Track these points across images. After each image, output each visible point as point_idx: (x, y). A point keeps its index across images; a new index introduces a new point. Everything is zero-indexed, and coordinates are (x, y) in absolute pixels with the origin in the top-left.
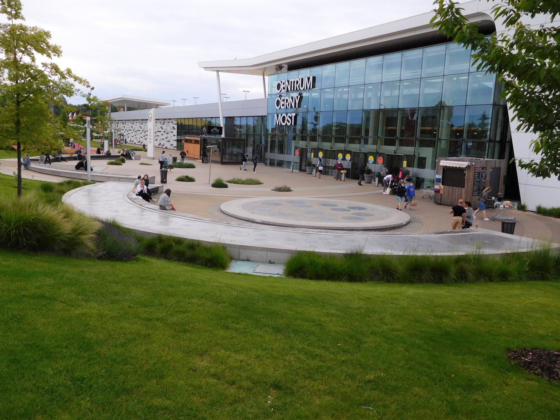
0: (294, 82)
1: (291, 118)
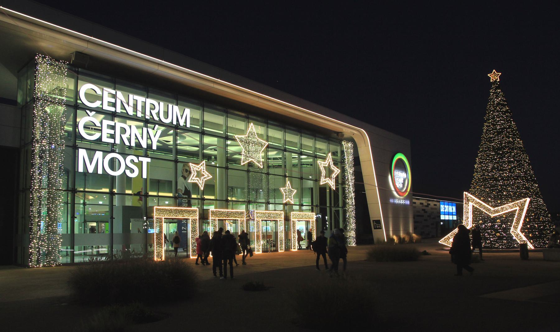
1: (140, 165)
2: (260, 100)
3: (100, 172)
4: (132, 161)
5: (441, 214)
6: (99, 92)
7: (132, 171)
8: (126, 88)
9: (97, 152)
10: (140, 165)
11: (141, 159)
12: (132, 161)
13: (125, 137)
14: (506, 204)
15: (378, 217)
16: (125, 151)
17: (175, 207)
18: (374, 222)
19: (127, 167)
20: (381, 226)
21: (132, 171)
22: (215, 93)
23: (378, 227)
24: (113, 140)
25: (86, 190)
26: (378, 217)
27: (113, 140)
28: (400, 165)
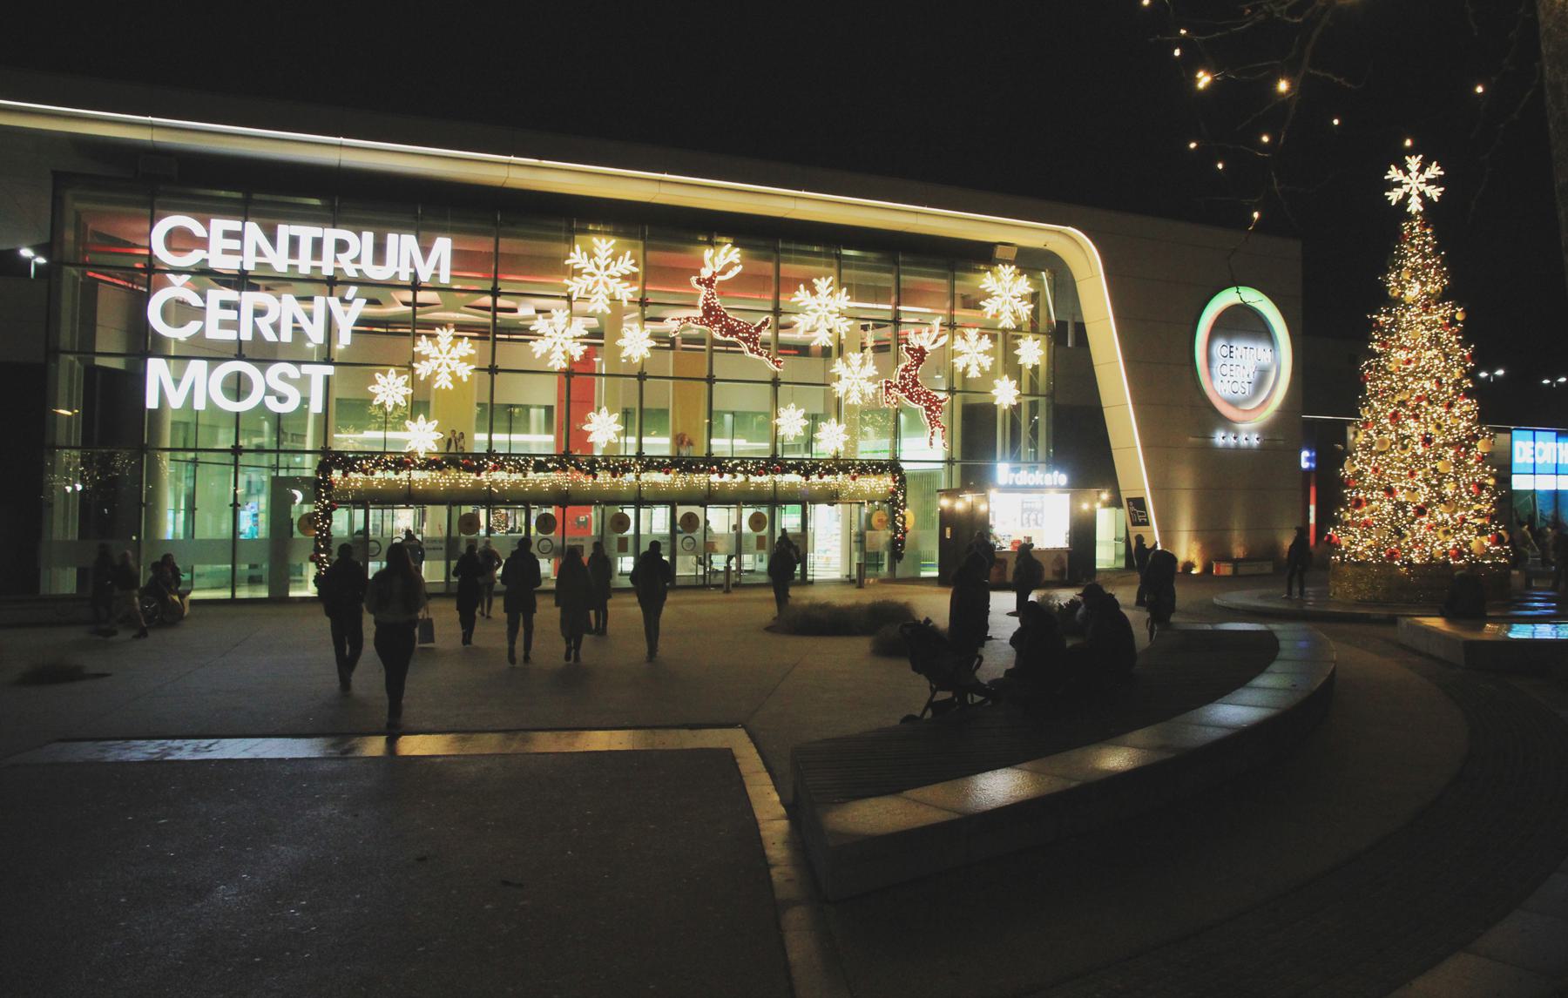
2: (665, 189)
3: (200, 404)
4: (283, 377)
5: (433, 562)
6: (197, 229)
7: (282, 399)
8: (535, 242)
9: (193, 362)
10: (303, 383)
11: (306, 368)
12: (283, 377)
13: (264, 324)
14: (702, 471)
15: (434, 549)
16: (262, 353)
17: (995, 451)
18: (1131, 503)
19: (269, 391)
20: (1147, 518)
21: (282, 399)
22: (473, 182)
23: (1140, 520)
24: (235, 332)
25: (309, 446)
26: (434, 549)
27: (235, 332)
28: (1241, 323)
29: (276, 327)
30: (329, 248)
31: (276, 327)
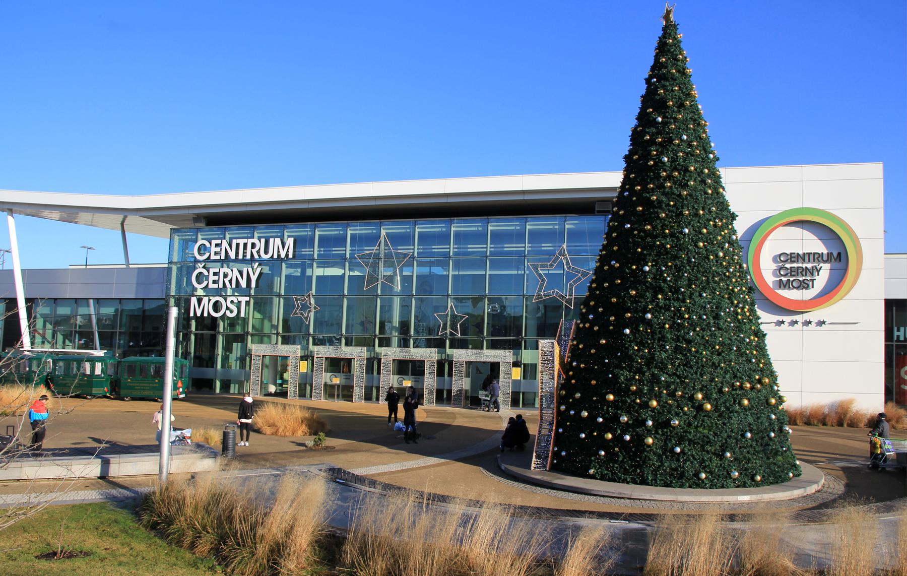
0: (245, 245)
7: (231, 312)
13: (227, 281)
19: (227, 308)
21: (231, 312)
29: (230, 281)
30: (249, 246)
31: (230, 281)
